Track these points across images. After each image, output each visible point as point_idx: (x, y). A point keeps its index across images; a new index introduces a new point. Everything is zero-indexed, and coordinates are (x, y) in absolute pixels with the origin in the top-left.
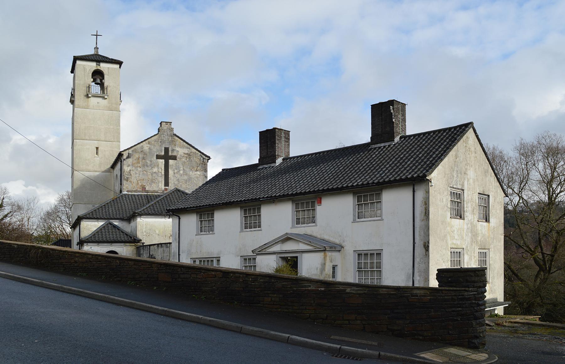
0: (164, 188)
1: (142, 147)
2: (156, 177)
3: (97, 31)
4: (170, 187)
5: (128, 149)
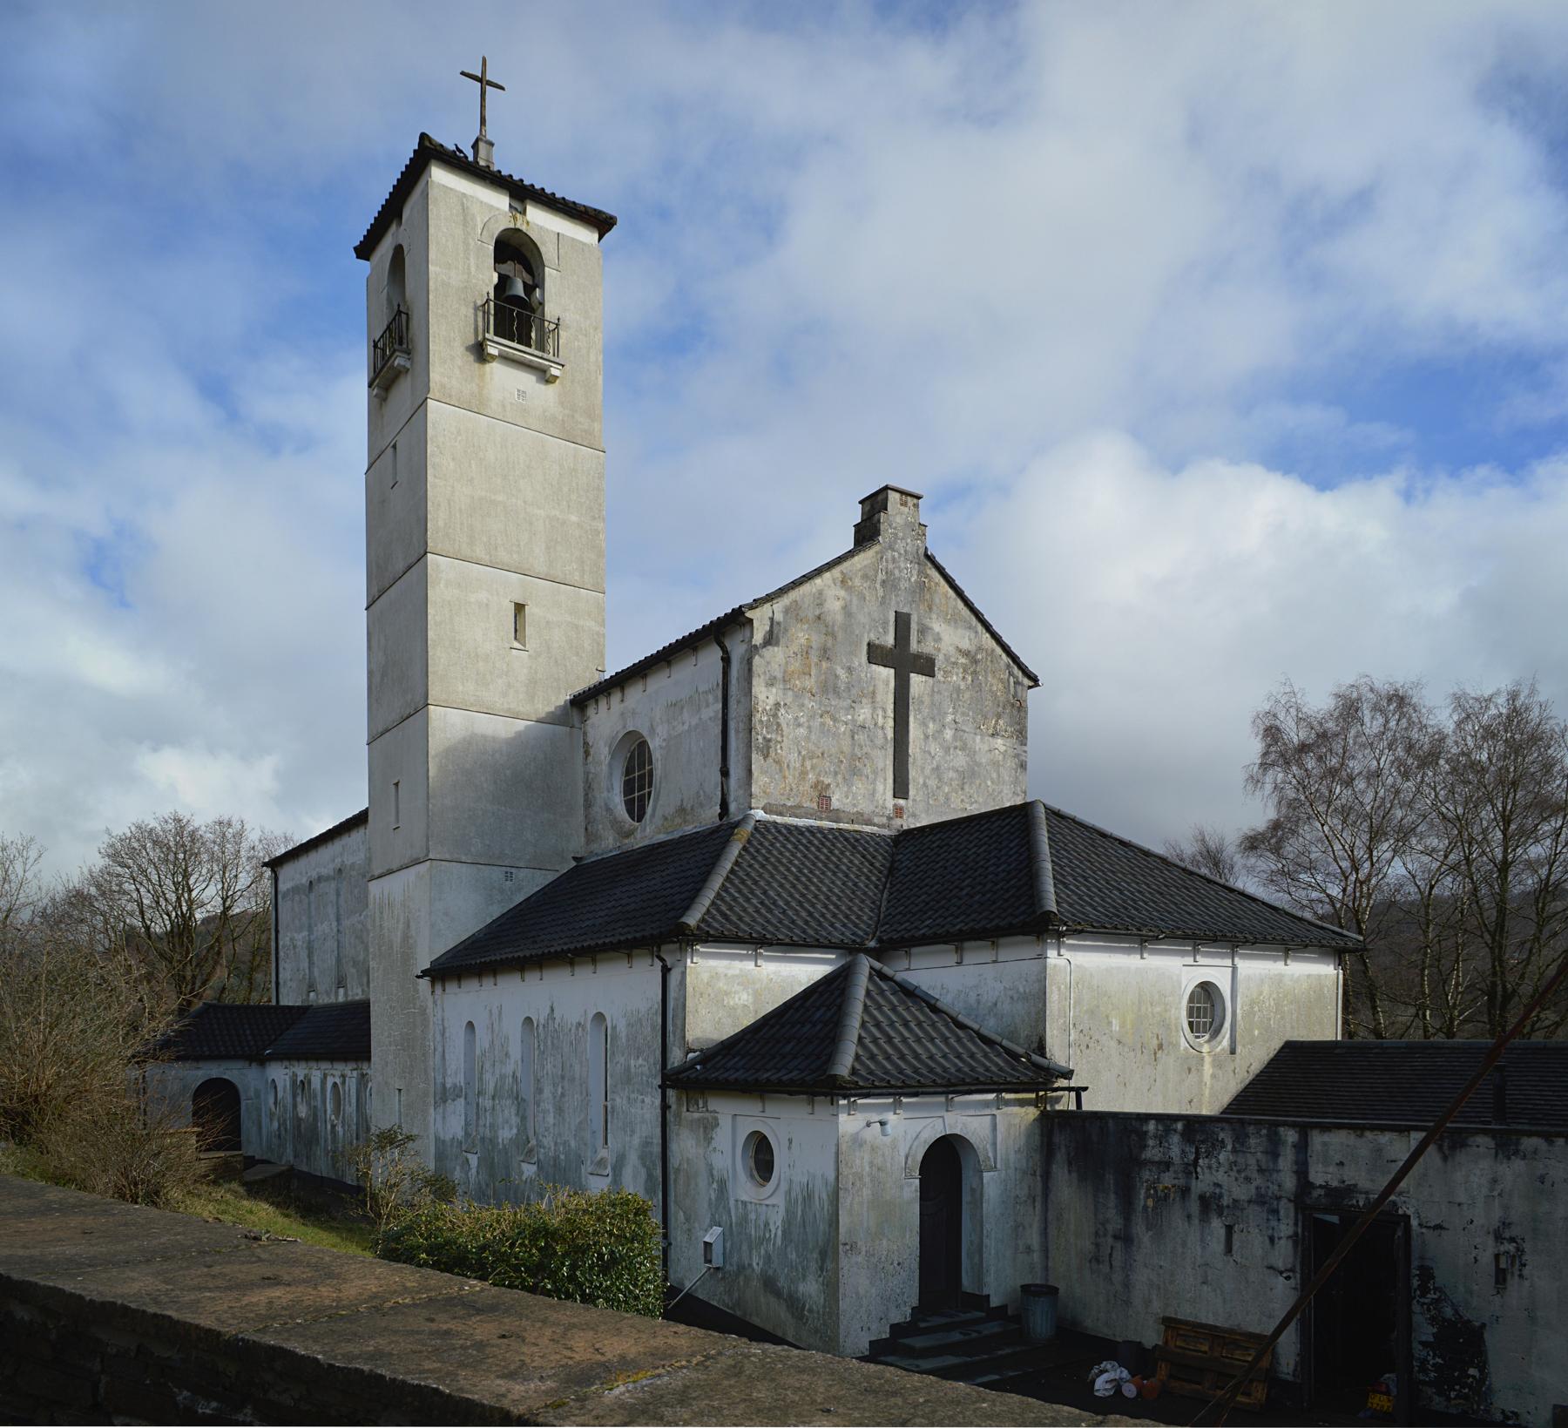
0: (893, 803)
1: (820, 600)
2: (865, 750)
3: (484, 60)
4: (910, 801)
5: (769, 598)
